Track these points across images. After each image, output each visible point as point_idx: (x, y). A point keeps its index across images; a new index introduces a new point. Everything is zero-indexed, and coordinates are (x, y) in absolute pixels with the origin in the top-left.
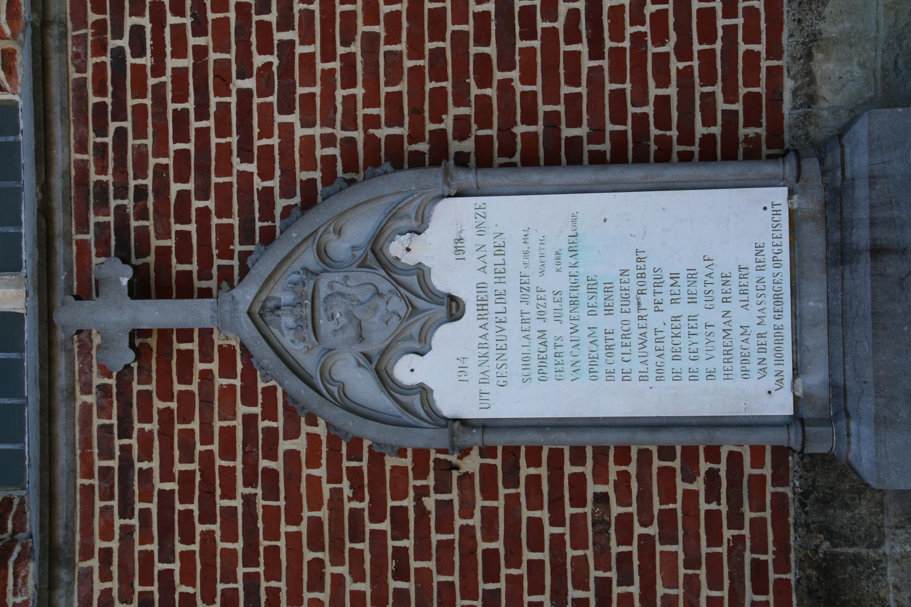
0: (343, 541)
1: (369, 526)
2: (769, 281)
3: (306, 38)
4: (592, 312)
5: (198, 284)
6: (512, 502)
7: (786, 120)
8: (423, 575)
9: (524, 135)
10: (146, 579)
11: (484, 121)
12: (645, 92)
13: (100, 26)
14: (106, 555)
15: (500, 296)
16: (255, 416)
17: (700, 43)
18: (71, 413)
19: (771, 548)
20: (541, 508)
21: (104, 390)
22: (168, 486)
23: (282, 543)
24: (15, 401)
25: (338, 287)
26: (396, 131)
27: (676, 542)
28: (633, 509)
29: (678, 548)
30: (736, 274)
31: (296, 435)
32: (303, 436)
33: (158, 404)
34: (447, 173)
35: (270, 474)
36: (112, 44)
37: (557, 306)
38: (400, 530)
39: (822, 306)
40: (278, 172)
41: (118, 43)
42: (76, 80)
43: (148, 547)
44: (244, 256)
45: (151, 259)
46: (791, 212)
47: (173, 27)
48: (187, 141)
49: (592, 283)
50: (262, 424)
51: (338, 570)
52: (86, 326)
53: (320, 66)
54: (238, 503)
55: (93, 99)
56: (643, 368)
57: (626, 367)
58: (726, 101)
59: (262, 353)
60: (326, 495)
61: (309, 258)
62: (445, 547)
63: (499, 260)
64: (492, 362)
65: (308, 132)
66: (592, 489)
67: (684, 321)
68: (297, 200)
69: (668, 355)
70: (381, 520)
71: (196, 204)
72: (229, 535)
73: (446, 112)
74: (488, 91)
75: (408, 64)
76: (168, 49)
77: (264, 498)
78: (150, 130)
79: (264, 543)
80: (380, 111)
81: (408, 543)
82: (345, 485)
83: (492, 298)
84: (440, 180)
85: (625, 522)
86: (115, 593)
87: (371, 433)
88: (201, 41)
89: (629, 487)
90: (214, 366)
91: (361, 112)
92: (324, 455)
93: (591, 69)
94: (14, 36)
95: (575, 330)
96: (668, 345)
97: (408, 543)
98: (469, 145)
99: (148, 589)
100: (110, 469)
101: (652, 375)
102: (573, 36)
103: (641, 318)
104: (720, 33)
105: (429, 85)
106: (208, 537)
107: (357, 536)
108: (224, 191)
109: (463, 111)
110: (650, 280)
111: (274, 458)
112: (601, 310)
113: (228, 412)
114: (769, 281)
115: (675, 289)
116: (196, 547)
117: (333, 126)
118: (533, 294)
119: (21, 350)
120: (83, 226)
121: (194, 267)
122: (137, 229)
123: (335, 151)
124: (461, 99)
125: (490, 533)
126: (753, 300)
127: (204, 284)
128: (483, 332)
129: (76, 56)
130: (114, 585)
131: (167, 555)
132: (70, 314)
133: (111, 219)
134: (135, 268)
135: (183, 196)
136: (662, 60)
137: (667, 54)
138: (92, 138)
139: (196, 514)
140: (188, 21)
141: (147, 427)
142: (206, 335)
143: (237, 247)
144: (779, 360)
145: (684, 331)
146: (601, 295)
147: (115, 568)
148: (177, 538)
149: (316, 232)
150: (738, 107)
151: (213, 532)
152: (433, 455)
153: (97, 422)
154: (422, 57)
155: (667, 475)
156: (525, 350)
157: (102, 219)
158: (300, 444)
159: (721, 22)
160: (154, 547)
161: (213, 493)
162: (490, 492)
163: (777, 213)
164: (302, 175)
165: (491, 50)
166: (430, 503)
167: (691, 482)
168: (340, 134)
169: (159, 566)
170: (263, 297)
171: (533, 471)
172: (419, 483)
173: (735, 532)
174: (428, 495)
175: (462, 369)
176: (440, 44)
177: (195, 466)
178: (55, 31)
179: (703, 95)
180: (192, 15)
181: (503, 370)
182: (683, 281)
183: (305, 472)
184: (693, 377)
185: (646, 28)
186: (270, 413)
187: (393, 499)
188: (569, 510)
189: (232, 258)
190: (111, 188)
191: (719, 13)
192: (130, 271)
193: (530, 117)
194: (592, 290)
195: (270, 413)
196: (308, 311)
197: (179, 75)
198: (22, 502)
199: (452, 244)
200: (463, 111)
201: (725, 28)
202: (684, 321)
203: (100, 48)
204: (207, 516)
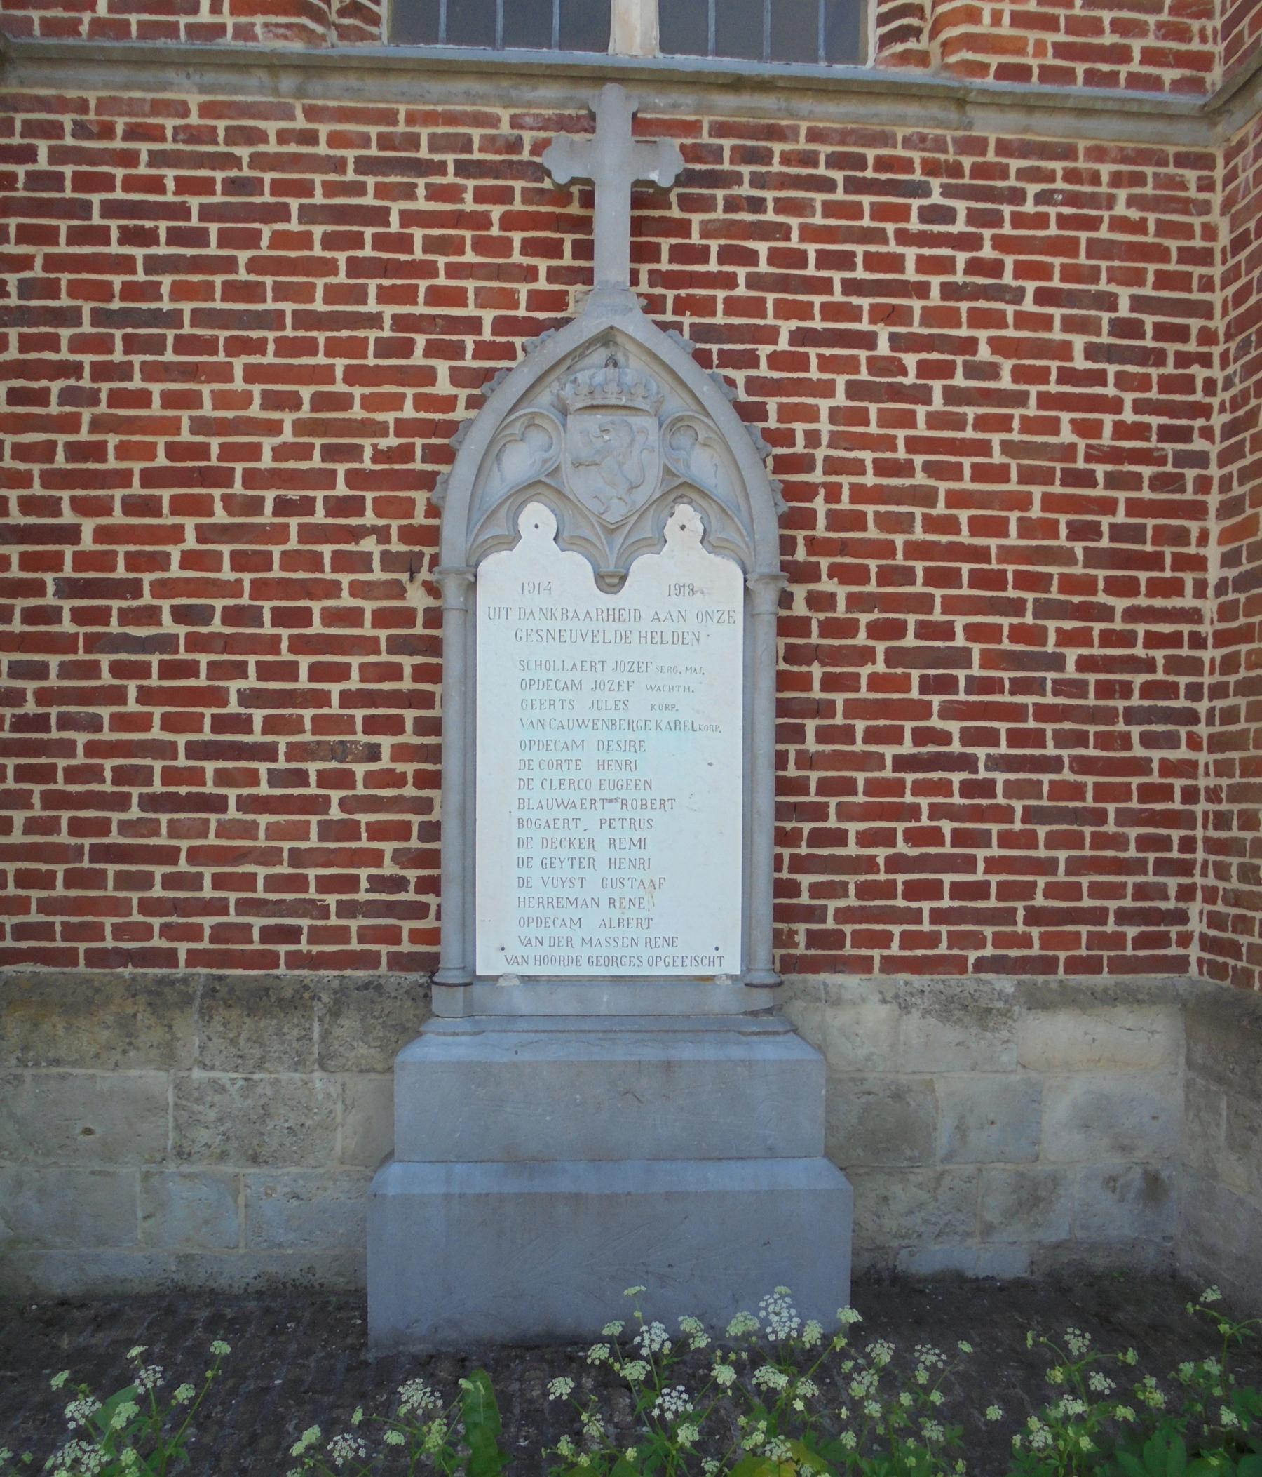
0: (324, 435)
1: (341, 469)
2: (631, 951)
3: (935, 420)
4: (604, 745)
5: (644, 268)
6: (370, 645)
7: (811, 977)
8: (280, 534)
9: (810, 674)
10: (279, 188)
11: (829, 628)
12: (851, 818)
13: (956, 170)
14: (309, 138)
15: (624, 637)
16: (480, 333)
17: (905, 883)
18: (485, 99)
19: (315, 949)
20: (362, 680)
21: (514, 146)
22: (394, 219)
23: (321, 359)
24: (499, 34)
25: (640, 438)
26: (821, 521)
27: (321, 839)
28: (360, 790)
29: (314, 842)
30: (644, 914)
31: (455, 382)
32: (453, 391)
33: (496, 212)
34: (775, 578)
35: (406, 348)
36: (936, 183)
37: (611, 704)
38: (338, 507)
39: (603, 1010)
40: (777, 375)
41: (936, 191)
42: (894, 136)
43: (318, 191)
44: (678, 326)
45: (676, 213)
46: (711, 978)
47: (953, 259)
48: (818, 267)
49: (636, 746)
50: (469, 341)
51: (288, 428)
52: (599, 124)
53: (901, 434)
54: (372, 306)
55: (871, 154)
56: (534, 804)
57: (536, 784)
58: (837, 910)
59: (559, 343)
60: (380, 417)
61: (676, 404)
62: (315, 562)
63: (668, 637)
64: (545, 625)
65: (824, 415)
66: (386, 742)
67: (588, 853)
68: (743, 397)
69: (549, 833)
70: (348, 484)
71: (742, 272)
72: (332, 294)
73: (841, 583)
74: (862, 634)
75: (899, 540)
76: (927, 252)
77: (378, 340)
78: (832, 222)
79: (321, 337)
80: (845, 504)
81: (320, 517)
82: (391, 441)
83: (622, 627)
84: (765, 570)
85: (343, 779)
86: (262, 148)
87: (461, 473)
88: (935, 292)
89: (388, 786)
90: (542, 284)
91: (845, 481)
92: (429, 416)
93: (882, 756)
94: (946, 67)
95: (582, 724)
96: (560, 833)
97: (320, 517)
98: (800, 608)
99: (267, 189)
100: (417, 147)
101: (525, 814)
102: (921, 737)
103: (593, 802)
104: (914, 905)
105: (873, 565)
106: (328, 267)
107: (330, 453)
108: (757, 308)
109: (841, 603)
110: (638, 814)
111: (427, 354)
112: (604, 755)
113: (484, 299)
114: (631, 951)
115: (626, 844)
116: (318, 251)
117: (830, 446)
118: (626, 676)
119: (561, 47)
120: (721, 130)
121: (665, 265)
122: (714, 197)
123: (800, 447)
124: (855, 602)
125: (331, 617)
126: (611, 934)
127: (643, 277)
128: (582, 615)
129: (923, 138)
130: (272, 147)
131: (308, 214)
132: (614, 107)
133: (726, 166)
134: (669, 190)
135: (750, 258)
136: (887, 838)
137: (894, 845)
138: (824, 150)
139: (359, 253)
140: (959, 278)
141: (469, 196)
142: (586, 277)
143: (687, 320)
144: (540, 961)
145: (576, 853)
146: (621, 757)
147: (293, 148)
148: (330, 228)
149: (708, 415)
150: (830, 924)
151: (336, 274)
152: (428, 551)
153: (476, 133)
154: (906, 557)
155: (403, 831)
156: (559, 664)
157: (727, 154)
158: (443, 387)
159: (926, 906)
160: (319, 199)
161: (385, 275)
162: (381, 619)
163: (711, 962)
164: (772, 404)
165: (910, 641)
166: (369, 544)
167: (394, 859)
168: (820, 454)
169: (294, 204)
170: (630, 347)
171: (407, 671)
172: (394, 532)
173: (333, 909)
174: (379, 542)
175: (536, 588)
176: (920, 580)
177: (418, 254)
178: (953, 115)
179: (845, 884)
180: (965, 285)
181: (534, 637)
182: (636, 853)
183: (410, 392)
184: (523, 862)
185: (925, 821)
186: (483, 350)
187: (375, 500)
188: (359, 714)
189: (675, 312)
190: (764, 169)
191: (936, 904)
192: (666, 182)
193: (830, 683)
194: (630, 745)
195: (483, 350)
196: (613, 402)
197: (896, 263)
198: (373, 37)
199: (687, 581)
200: (841, 603)
201: (920, 910)
202: (588, 853)
203: (932, 168)
204: (355, 267)
